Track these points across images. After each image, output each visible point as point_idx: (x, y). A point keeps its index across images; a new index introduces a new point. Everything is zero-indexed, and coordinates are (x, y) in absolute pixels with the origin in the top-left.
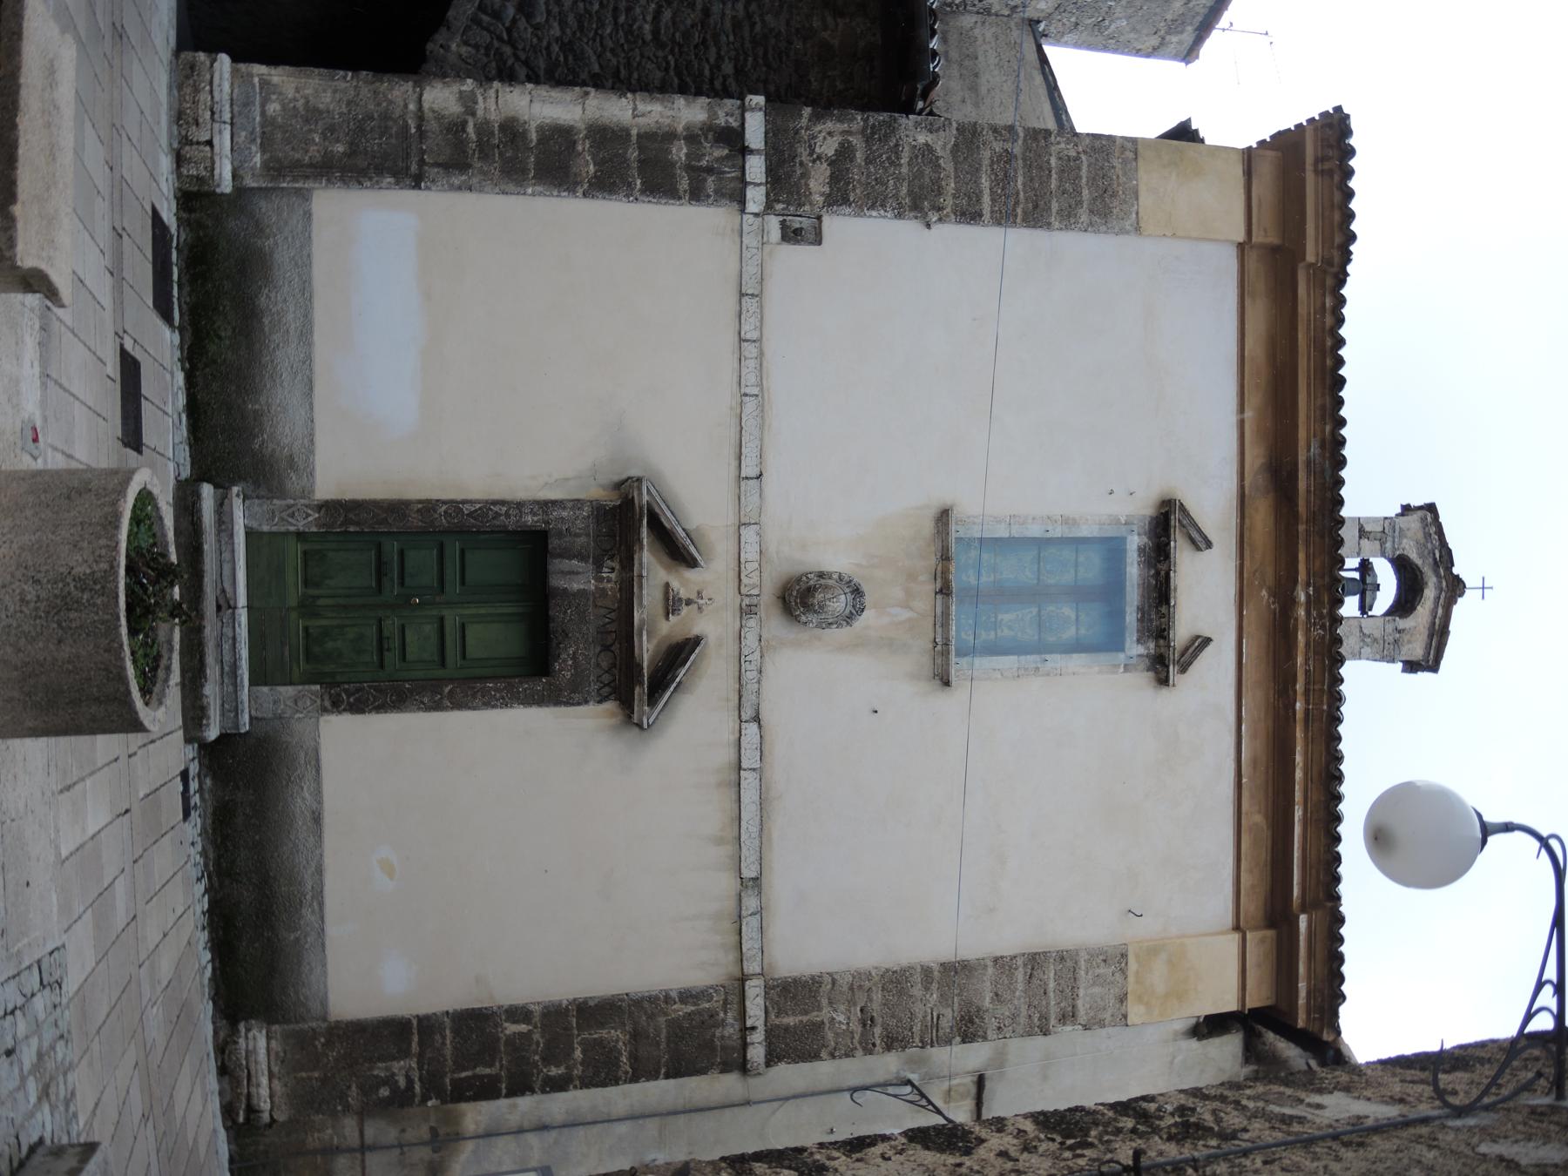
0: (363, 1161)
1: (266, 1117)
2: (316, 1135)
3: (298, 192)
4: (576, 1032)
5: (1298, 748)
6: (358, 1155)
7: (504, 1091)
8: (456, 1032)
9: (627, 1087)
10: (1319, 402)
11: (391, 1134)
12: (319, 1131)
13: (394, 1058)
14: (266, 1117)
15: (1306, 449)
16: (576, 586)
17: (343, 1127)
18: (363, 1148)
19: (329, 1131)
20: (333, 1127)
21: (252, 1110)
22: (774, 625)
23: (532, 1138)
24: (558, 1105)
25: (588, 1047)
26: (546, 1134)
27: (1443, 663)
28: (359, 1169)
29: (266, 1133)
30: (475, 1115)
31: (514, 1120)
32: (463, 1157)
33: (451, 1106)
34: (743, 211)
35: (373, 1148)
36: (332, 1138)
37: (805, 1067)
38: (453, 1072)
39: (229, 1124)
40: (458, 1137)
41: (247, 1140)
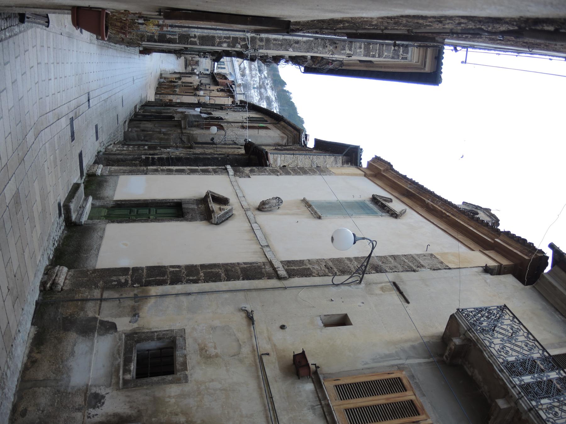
0: (100, 304)
1: (59, 288)
2: (80, 295)
3: (116, 175)
4: (200, 270)
5: (457, 219)
6: (99, 302)
7: (169, 283)
8: (146, 270)
9: (225, 282)
10: (403, 182)
11: (116, 295)
12: (82, 294)
13: (120, 275)
14: (59, 288)
15: (407, 187)
16: (191, 207)
17: (94, 292)
18: (101, 300)
19: (87, 294)
20: (89, 292)
21: (54, 284)
22: (257, 212)
23: (183, 299)
24: (194, 287)
25: (205, 273)
26: (190, 297)
27: (499, 218)
28: (98, 307)
29: (58, 294)
30: (154, 290)
31: (174, 292)
32: (149, 305)
33: (144, 287)
34: (229, 175)
35: (106, 300)
36: (87, 296)
37: (308, 278)
38: (146, 278)
39: (42, 288)
40: (147, 297)
41: (48, 296)
